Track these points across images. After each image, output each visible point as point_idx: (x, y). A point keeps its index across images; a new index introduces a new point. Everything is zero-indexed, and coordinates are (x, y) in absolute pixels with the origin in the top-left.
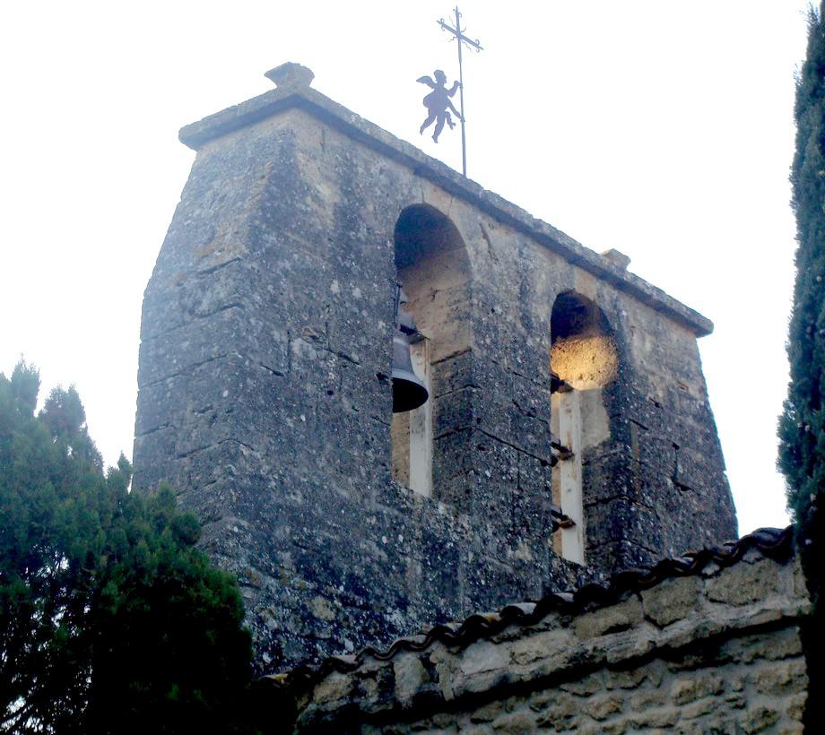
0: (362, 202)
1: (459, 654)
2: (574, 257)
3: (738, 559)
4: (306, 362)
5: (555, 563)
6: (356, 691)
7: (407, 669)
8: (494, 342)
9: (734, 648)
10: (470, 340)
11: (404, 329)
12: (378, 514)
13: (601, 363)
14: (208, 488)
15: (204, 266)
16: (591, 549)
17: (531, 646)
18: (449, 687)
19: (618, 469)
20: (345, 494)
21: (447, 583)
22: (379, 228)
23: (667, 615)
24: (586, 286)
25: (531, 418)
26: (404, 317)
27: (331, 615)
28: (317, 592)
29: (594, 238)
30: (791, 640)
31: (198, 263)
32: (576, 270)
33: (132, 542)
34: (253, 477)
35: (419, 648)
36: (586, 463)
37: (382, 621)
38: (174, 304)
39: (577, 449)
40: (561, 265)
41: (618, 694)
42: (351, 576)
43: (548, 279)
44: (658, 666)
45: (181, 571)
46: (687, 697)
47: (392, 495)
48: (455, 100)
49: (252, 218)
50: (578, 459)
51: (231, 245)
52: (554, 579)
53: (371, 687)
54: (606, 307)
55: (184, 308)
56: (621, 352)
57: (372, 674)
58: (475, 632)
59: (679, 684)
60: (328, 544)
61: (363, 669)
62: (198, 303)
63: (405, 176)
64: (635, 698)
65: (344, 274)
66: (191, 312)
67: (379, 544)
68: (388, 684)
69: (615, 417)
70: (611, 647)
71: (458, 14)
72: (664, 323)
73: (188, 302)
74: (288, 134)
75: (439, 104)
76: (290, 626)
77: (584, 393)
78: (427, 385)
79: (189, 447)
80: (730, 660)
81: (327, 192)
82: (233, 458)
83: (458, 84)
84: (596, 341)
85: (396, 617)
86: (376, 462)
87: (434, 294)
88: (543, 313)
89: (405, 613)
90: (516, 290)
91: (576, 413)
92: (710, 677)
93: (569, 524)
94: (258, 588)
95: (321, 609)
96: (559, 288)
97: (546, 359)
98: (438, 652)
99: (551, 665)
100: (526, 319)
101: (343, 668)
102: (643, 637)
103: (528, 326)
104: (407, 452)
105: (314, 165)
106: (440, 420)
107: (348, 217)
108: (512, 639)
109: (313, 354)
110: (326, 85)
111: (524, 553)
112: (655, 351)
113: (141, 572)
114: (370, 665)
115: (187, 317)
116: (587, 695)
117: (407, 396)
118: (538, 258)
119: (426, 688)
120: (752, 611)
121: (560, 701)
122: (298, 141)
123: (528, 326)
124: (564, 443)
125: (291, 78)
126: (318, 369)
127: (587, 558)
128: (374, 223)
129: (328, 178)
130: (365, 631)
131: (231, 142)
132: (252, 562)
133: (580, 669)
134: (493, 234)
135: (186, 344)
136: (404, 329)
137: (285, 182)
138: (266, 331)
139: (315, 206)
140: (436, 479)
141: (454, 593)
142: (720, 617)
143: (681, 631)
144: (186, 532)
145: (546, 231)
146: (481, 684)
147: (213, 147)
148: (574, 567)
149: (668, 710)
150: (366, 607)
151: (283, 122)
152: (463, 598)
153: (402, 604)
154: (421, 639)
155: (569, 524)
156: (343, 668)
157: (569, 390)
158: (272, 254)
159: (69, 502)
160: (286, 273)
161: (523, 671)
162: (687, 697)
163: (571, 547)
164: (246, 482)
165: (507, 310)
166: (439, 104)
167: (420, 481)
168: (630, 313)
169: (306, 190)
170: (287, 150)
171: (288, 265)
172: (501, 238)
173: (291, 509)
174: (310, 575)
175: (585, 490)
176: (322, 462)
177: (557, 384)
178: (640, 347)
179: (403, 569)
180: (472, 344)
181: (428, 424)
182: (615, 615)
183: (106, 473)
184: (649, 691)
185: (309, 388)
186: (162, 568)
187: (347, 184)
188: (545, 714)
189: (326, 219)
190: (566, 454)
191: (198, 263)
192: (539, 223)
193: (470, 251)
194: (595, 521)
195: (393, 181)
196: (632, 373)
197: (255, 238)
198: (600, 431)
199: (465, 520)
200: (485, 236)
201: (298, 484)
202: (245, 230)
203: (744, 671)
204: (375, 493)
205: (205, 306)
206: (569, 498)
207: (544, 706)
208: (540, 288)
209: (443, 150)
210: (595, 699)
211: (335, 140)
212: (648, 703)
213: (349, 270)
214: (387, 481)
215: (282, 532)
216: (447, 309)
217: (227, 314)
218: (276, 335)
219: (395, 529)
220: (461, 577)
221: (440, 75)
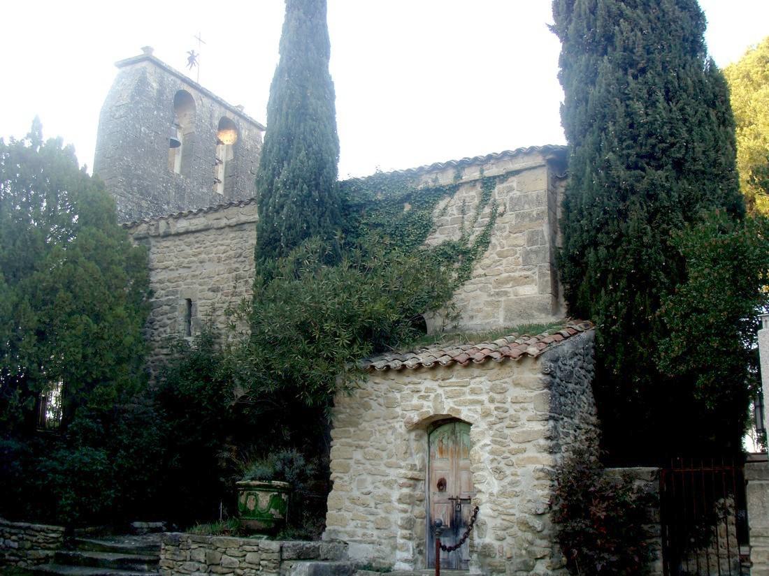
0: (166, 89)
1: (176, 221)
2: (227, 107)
3: (250, 203)
4: (145, 134)
5: (214, 193)
6: (149, 229)
7: (162, 224)
8: (201, 131)
9: (246, 226)
10: (194, 130)
11: (176, 125)
12: (163, 178)
13: (233, 137)
14: (115, 168)
15: (117, 105)
16: (225, 190)
17: (195, 221)
18: (173, 231)
19: (235, 168)
20: (154, 172)
21: (182, 198)
22: (170, 95)
23: (230, 216)
24: (229, 115)
25: (213, 152)
26: (176, 121)
27: (147, 206)
28: (143, 199)
29: (232, 101)
30: (254, 227)
31: (116, 103)
32: (228, 111)
33: (85, 189)
34: (127, 166)
35: (166, 219)
36: (226, 165)
37: (161, 208)
38: (108, 114)
39: (224, 161)
40: (223, 109)
41: (216, 236)
42: (154, 195)
43: (218, 113)
44: (227, 229)
45: (98, 197)
46: (233, 239)
47: (168, 172)
48: (196, 59)
49: (132, 92)
50: (224, 164)
51: (126, 99)
52: (213, 198)
53: (152, 228)
54: (235, 122)
55: (111, 116)
56: (239, 134)
57: (153, 225)
58: (181, 216)
59: (232, 235)
60: (148, 185)
61: (151, 223)
62: (115, 115)
63: (179, 82)
64: (221, 238)
65: (158, 109)
66: (113, 117)
67: (163, 186)
68: (157, 228)
69: (235, 153)
70: (216, 224)
71: (200, 33)
72: (252, 127)
73: (112, 114)
74: (145, 68)
75: (192, 60)
76: (135, 208)
77: (228, 145)
78: (181, 142)
79: (110, 156)
80: (245, 230)
81: (155, 85)
82: (122, 160)
83: (198, 54)
84: (232, 131)
85: (166, 207)
86: (164, 163)
87: (185, 115)
88: (216, 123)
89: (168, 206)
90: (209, 116)
91: (225, 151)
92: (239, 234)
93: (220, 182)
94: (126, 197)
95: (144, 204)
96: (222, 115)
97: (216, 135)
98: (171, 221)
99: (200, 227)
100: (211, 124)
101: (146, 223)
102: (223, 222)
103: (212, 126)
104: (174, 159)
105: (152, 77)
106: (184, 151)
107: (161, 92)
108: (190, 219)
109: (147, 132)
110: (157, 54)
111: (205, 190)
112: (249, 135)
113: (87, 197)
114: (152, 223)
115: (112, 119)
116: (208, 236)
117: (175, 144)
118: (216, 107)
119: (167, 230)
120: (252, 217)
121: (201, 236)
122: (148, 70)
123: (212, 126)
124: (220, 159)
125: (147, 49)
126: (148, 136)
127: (224, 192)
128: (168, 95)
129: (155, 81)
130: (156, 210)
131: (128, 68)
132: (125, 190)
133: (206, 229)
134: (203, 99)
135: (111, 126)
136: (176, 125)
137: (143, 82)
138: (134, 125)
139: (152, 90)
140: (182, 167)
141: (183, 200)
142: (243, 219)
143: (233, 221)
144: (38, 294)
145: (219, 99)
146: (181, 231)
147: (124, 69)
148: (219, 194)
149: (229, 241)
150: (157, 204)
151: (144, 64)
152: (186, 202)
153: (168, 203)
154: (167, 217)
155: (220, 182)
156: (146, 223)
157: (223, 144)
158: (137, 103)
159: (68, 177)
160: (141, 108)
161: (193, 228)
162: (233, 239)
163: (220, 189)
164: (125, 167)
165: (205, 121)
166: (192, 60)
167: (177, 170)
168: (242, 123)
169: (149, 84)
170: (144, 73)
171: (142, 106)
172: (205, 100)
173: (138, 175)
174: (142, 194)
175: (225, 173)
176: (148, 162)
177: (219, 142)
178: (244, 133)
179: (169, 193)
180: (194, 130)
181: (180, 152)
182: (217, 215)
183: (80, 169)
184: (224, 236)
185: (145, 141)
186: (93, 196)
187: (161, 83)
188: (197, 239)
189: (154, 93)
190: (221, 162)
191: (116, 103)
192: (217, 97)
193: (196, 104)
194: (227, 181)
195: (175, 82)
196: (241, 141)
197: (132, 98)
198: (231, 156)
199: (188, 181)
200: (201, 100)
201: (140, 169)
202: (130, 95)
203: (248, 233)
204: (163, 172)
205: (117, 116)
206: (221, 173)
207: (197, 237)
208: (216, 115)
209: (192, 75)
210: (210, 237)
211: (158, 70)
212: (224, 239)
213: (159, 108)
214: (166, 168)
215: (135, 181)
216: (188, 120)
217: (123, 119)
218: (137, 126)
219: (167, 182)
220: (186, 196)
221: (193, 51)
